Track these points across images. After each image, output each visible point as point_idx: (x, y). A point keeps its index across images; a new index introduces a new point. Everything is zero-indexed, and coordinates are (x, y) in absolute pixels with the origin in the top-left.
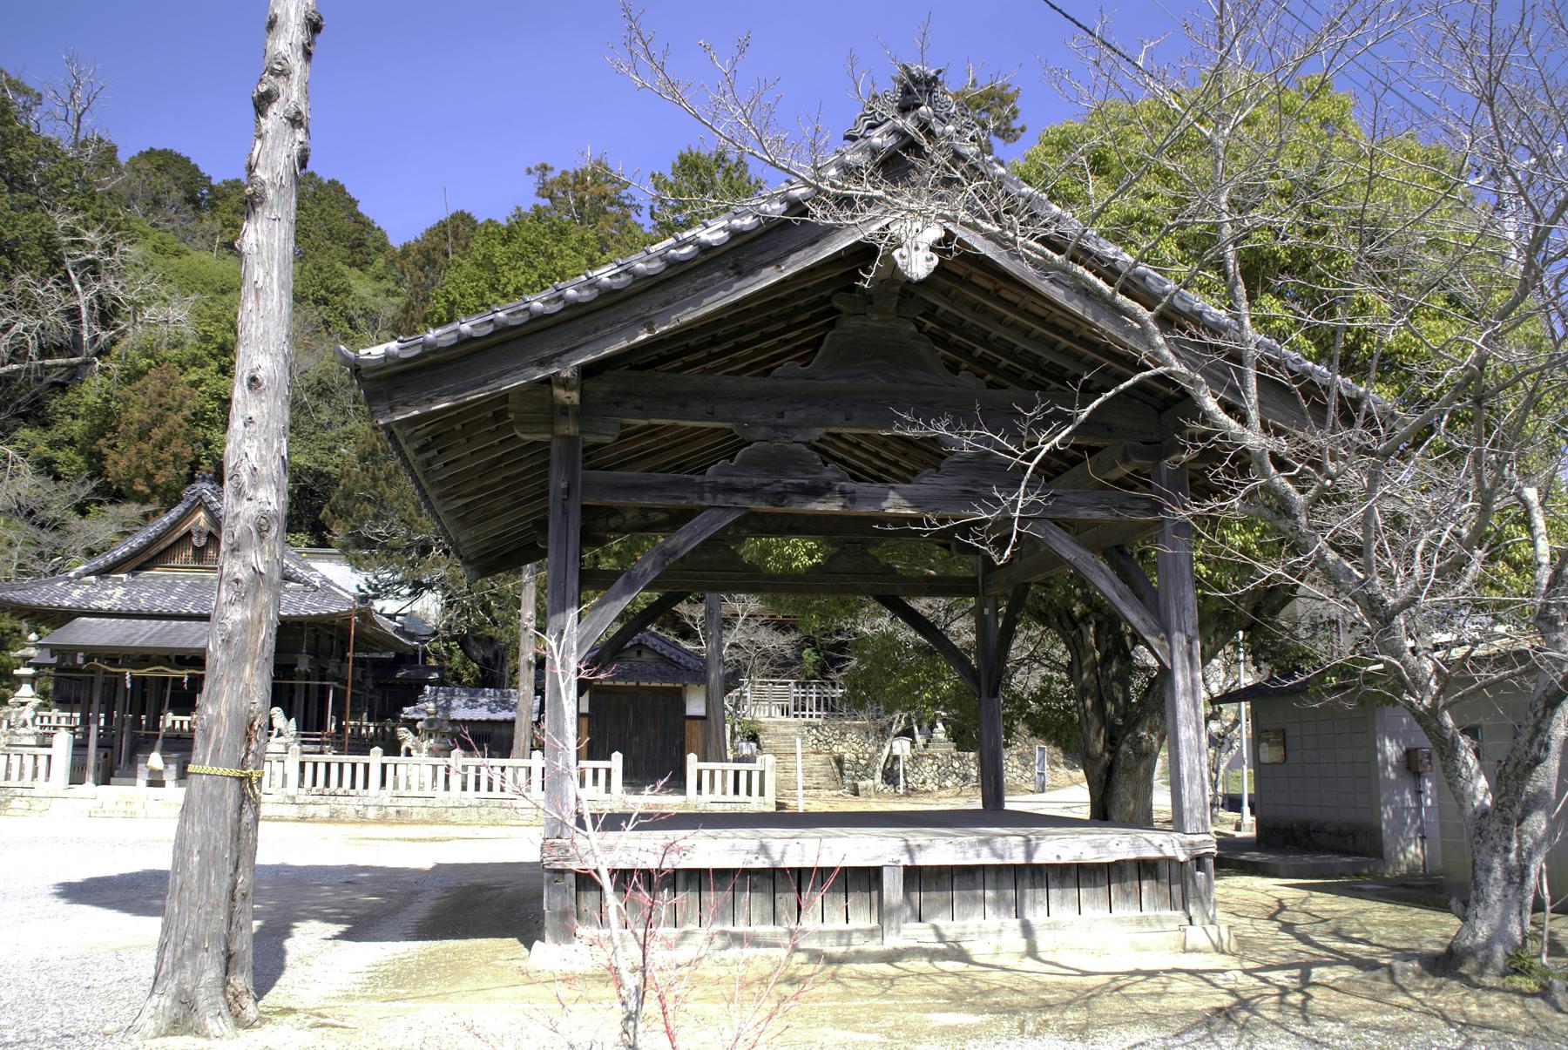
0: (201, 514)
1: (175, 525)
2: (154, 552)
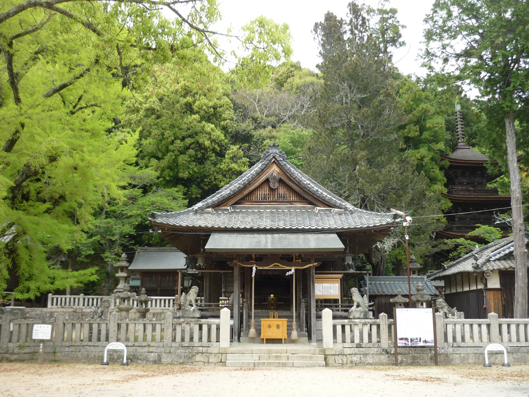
0: (275, 168)
1: (259, 174)
2: (246, 192)
